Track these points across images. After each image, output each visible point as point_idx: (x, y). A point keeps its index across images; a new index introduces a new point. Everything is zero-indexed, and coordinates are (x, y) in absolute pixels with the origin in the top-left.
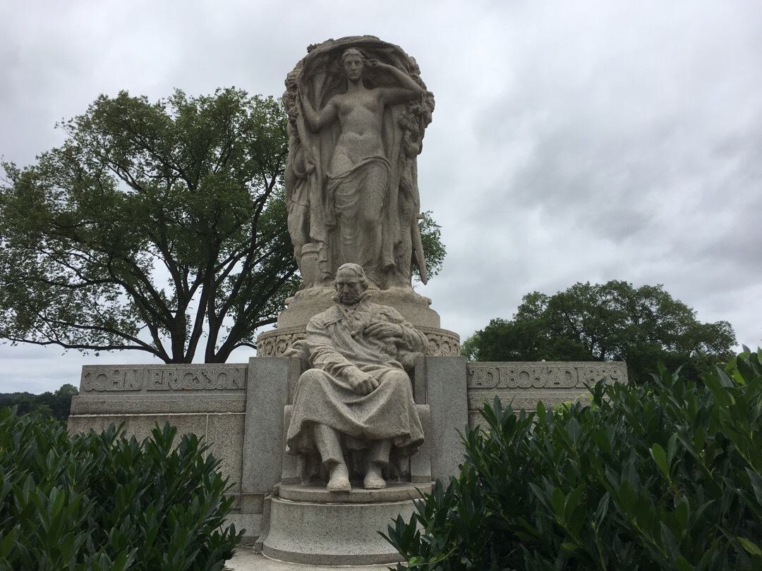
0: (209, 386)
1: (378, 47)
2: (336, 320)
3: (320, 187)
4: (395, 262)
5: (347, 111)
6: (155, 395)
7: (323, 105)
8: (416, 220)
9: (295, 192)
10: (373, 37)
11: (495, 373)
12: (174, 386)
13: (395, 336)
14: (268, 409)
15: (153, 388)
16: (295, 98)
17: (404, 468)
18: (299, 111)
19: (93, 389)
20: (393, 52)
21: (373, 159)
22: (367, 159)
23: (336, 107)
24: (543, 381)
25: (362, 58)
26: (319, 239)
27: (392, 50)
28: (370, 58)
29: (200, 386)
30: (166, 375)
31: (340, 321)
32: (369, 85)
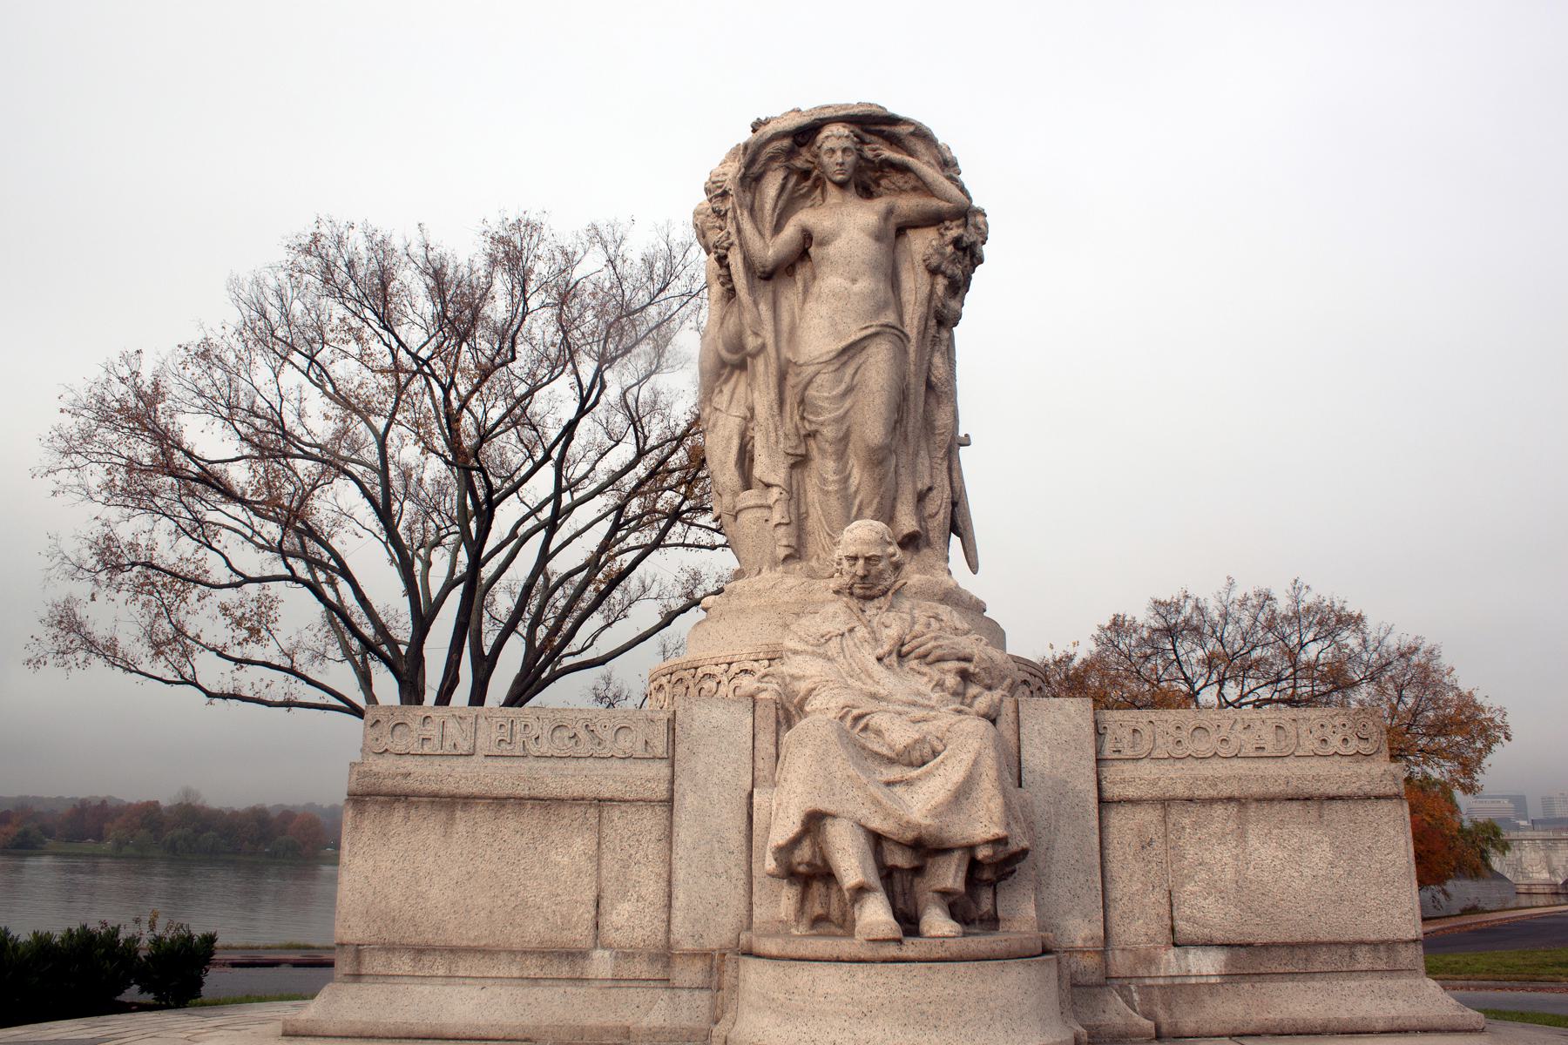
0: (598, 751)
1: (871, 124)
2: (844, 629)
3: (773, 381)
4: (921, 527)
6: (501, 763)
7: (778, 228)
8: (957, 446)
9: (721, 391)
11: (1146, 731)
12: (533, 749)
13: (959, 659)
14: (716, 796)
15: (496, 752)
16: (726, 214)
17: (986, 905)
18: (734, 238)
20: (913, 134)
21: (879, 329)
22: (866, 328)
23: (807, 237)
24: (1234, 743)
25: (856, 143)
26: (771, 481)
27: (911, 129)
28: (869, 143)
29: (582, 750)
31: (851, 630)
32: (866, 192)
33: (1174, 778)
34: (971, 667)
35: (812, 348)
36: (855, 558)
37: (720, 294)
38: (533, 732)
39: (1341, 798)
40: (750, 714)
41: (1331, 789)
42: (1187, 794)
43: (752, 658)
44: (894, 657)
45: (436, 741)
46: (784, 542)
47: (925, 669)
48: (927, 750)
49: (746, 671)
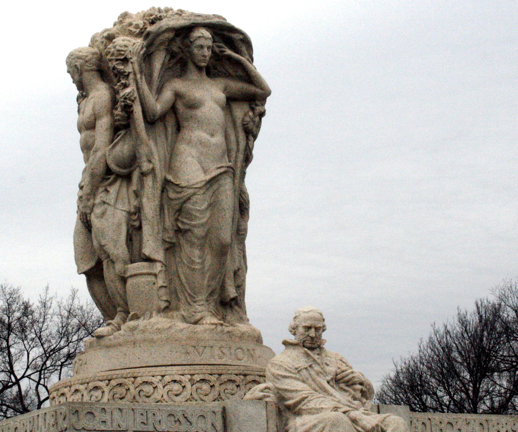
2: (307, 365)
5: (193, 106)
10: (219, 17)
11: (428, 423)
16: (128, 75)
19: (83, 428)
23: (178, 95)
30: (150, 415)
35: (190, 177)
38: (157, 418)
40: (265, 409)
43: (180, 373)
46: (164, 298)
49: (175, 381)
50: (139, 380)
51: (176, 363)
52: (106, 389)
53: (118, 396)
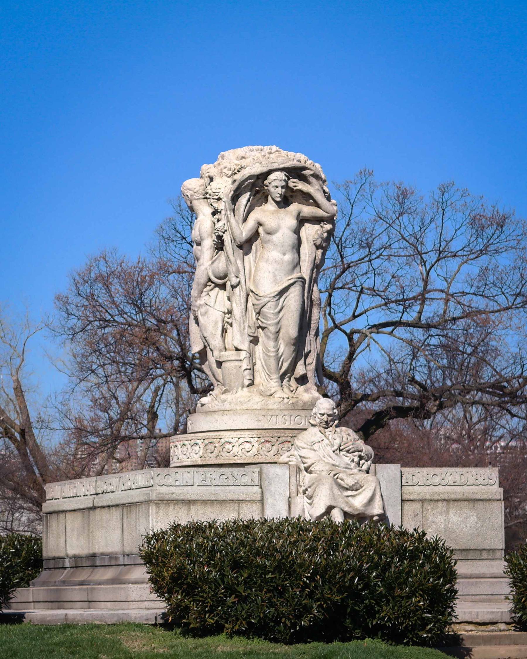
2: (320, 440)
7: (245, 220)
21: (296, 280)
29: (230, 482)
33: (426, 492)
34: (362, 454)
36: (323, 415)
37: (210, 246)
39: (482, 500)
41: (478, 497)
42: (430, 498)
44: (338, 450)
45: (180, 481)
46: (248, 378)
47: (348, 455)
48: (358, 486)
50: (223, 441)
51: (251, 428)
52: (202, 446)
53: (209, 451)
